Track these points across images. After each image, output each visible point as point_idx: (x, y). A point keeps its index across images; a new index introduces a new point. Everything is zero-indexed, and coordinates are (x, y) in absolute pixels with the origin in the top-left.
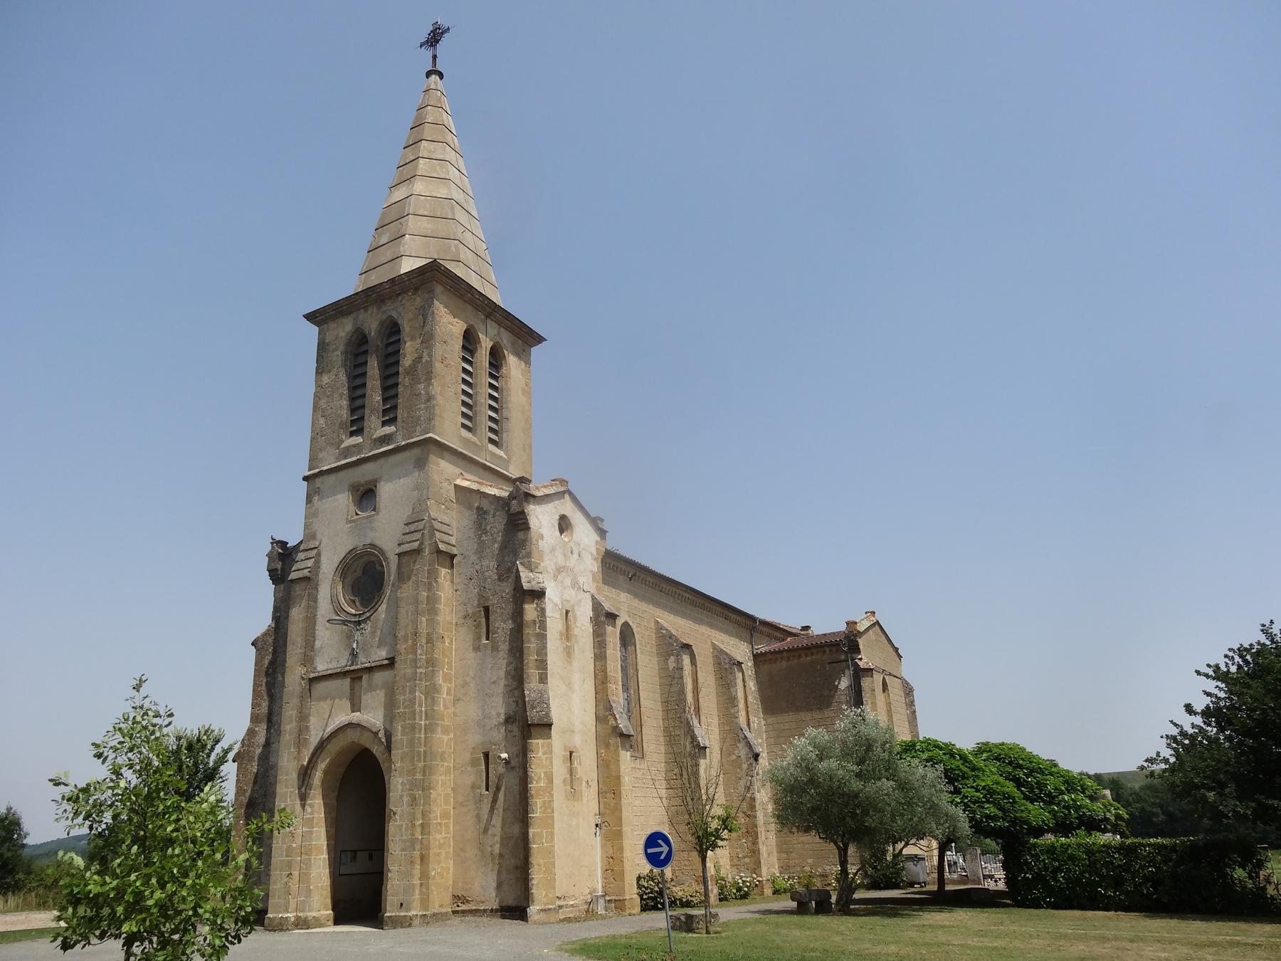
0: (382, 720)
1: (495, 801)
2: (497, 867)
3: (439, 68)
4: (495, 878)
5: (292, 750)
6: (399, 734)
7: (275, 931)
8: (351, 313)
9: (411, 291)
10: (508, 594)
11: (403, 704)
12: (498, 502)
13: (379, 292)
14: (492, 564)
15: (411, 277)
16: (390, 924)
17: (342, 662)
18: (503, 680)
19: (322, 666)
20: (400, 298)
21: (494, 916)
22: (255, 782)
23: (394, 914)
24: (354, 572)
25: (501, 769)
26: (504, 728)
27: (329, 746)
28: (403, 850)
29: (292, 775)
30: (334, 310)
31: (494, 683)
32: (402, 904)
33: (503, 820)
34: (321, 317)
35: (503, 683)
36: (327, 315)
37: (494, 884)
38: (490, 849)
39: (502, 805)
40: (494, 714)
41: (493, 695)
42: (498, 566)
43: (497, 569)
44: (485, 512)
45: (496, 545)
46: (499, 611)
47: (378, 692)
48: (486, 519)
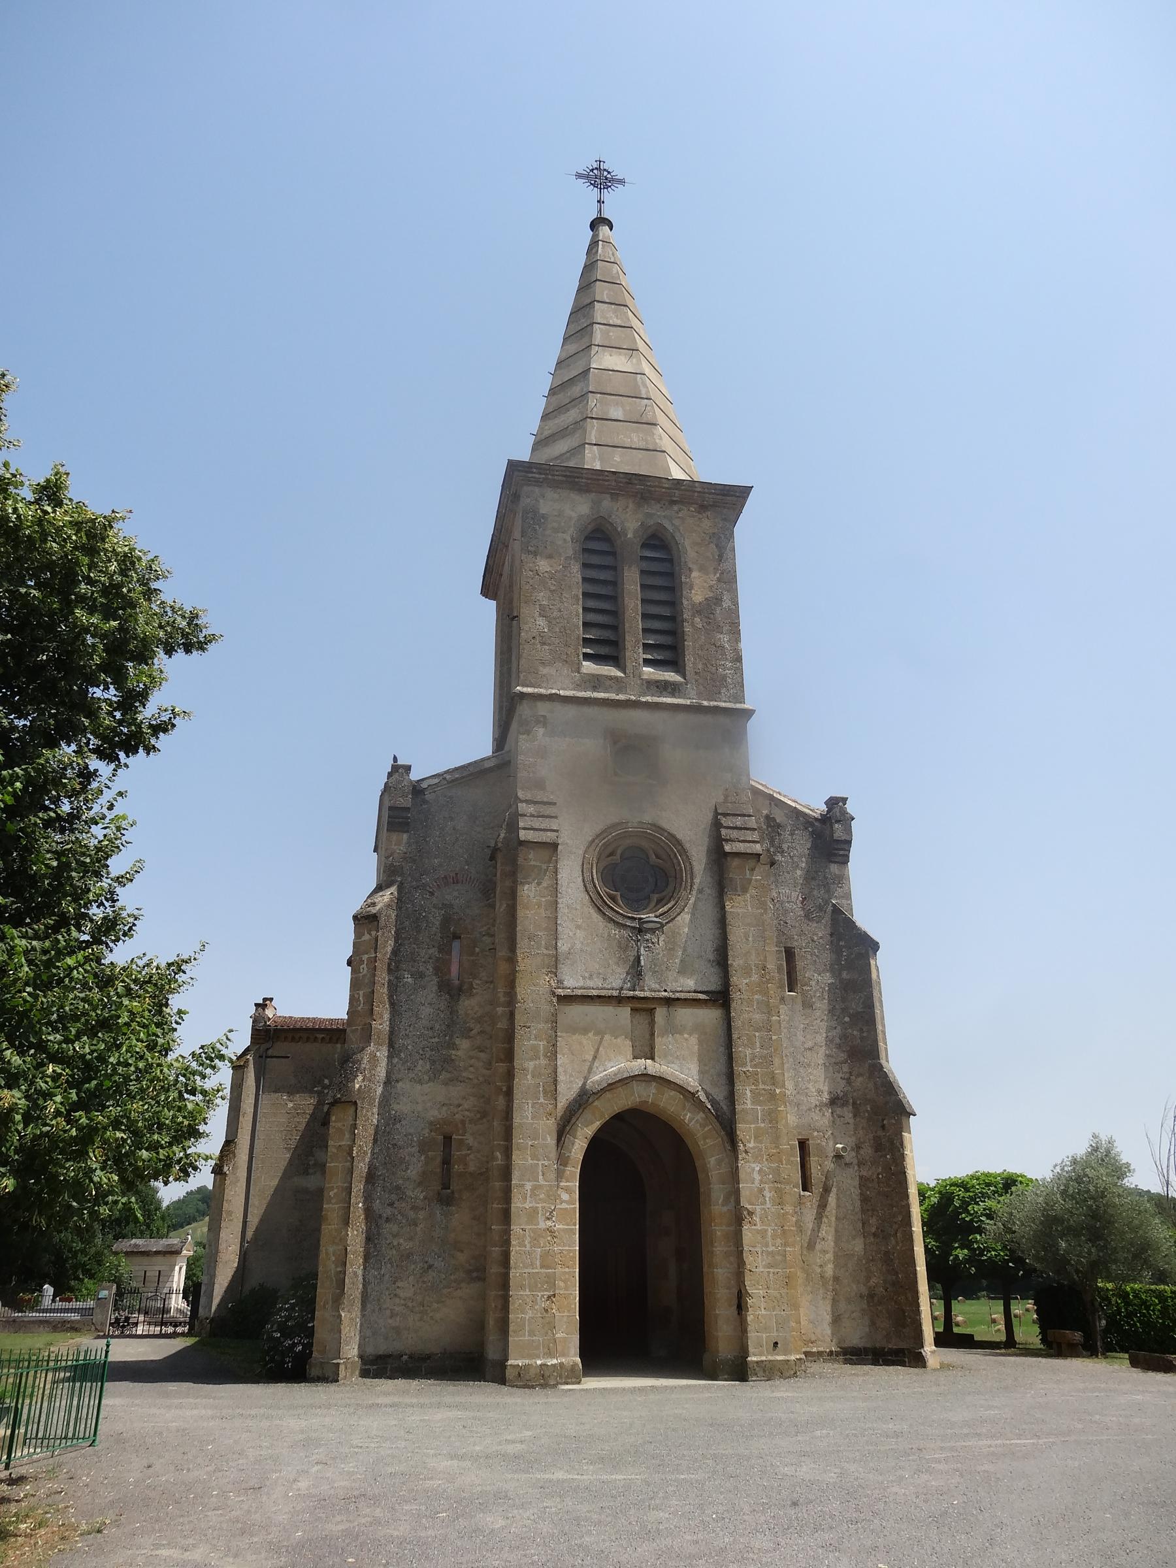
0: (697, 1077)
1: (822, 1206)
2: (830, 1295)
3: (605, 215)
4: (829, 1308)
5: (542, 1100)
6: (749, 1102)
7: (533, 1387)
8: (588, 491)
9: (695, 506)
10: (821, 938)
11: (751, 1061)
12: (797, 818)
13: (650, 486)
14: (794, 894)
15: (706, 490)
16: (761, 1373)
17: (615, 980)
18: (824, 1048)
19: (573, 982)
20: (676, 508)
21: (835, 1361)
22: (375, 1141)
23: (764, 1358)
24: (608, 856)
25: (829, 1165)
26: (830, 1111)
27: (596, 1103)
28: (770, 1266)
29: (544, 1139)
30: (565, 476)
31: (810, 1049)
32: (776, 1344)
33: (836, 1231)
34: (537, 476)
35: (822, 1051)
36: (550, 477)
37: (828, 1318)
38: (819, 1270)
39: (834, 1211)
40: (814, 1090)
41: (809, 1065)
42: (804, 899)
43: (802, 903)
44: (779, 826)
45: (799, 872)
46: (809, 957)
47: (686, 1036)
48: (779, 835)
